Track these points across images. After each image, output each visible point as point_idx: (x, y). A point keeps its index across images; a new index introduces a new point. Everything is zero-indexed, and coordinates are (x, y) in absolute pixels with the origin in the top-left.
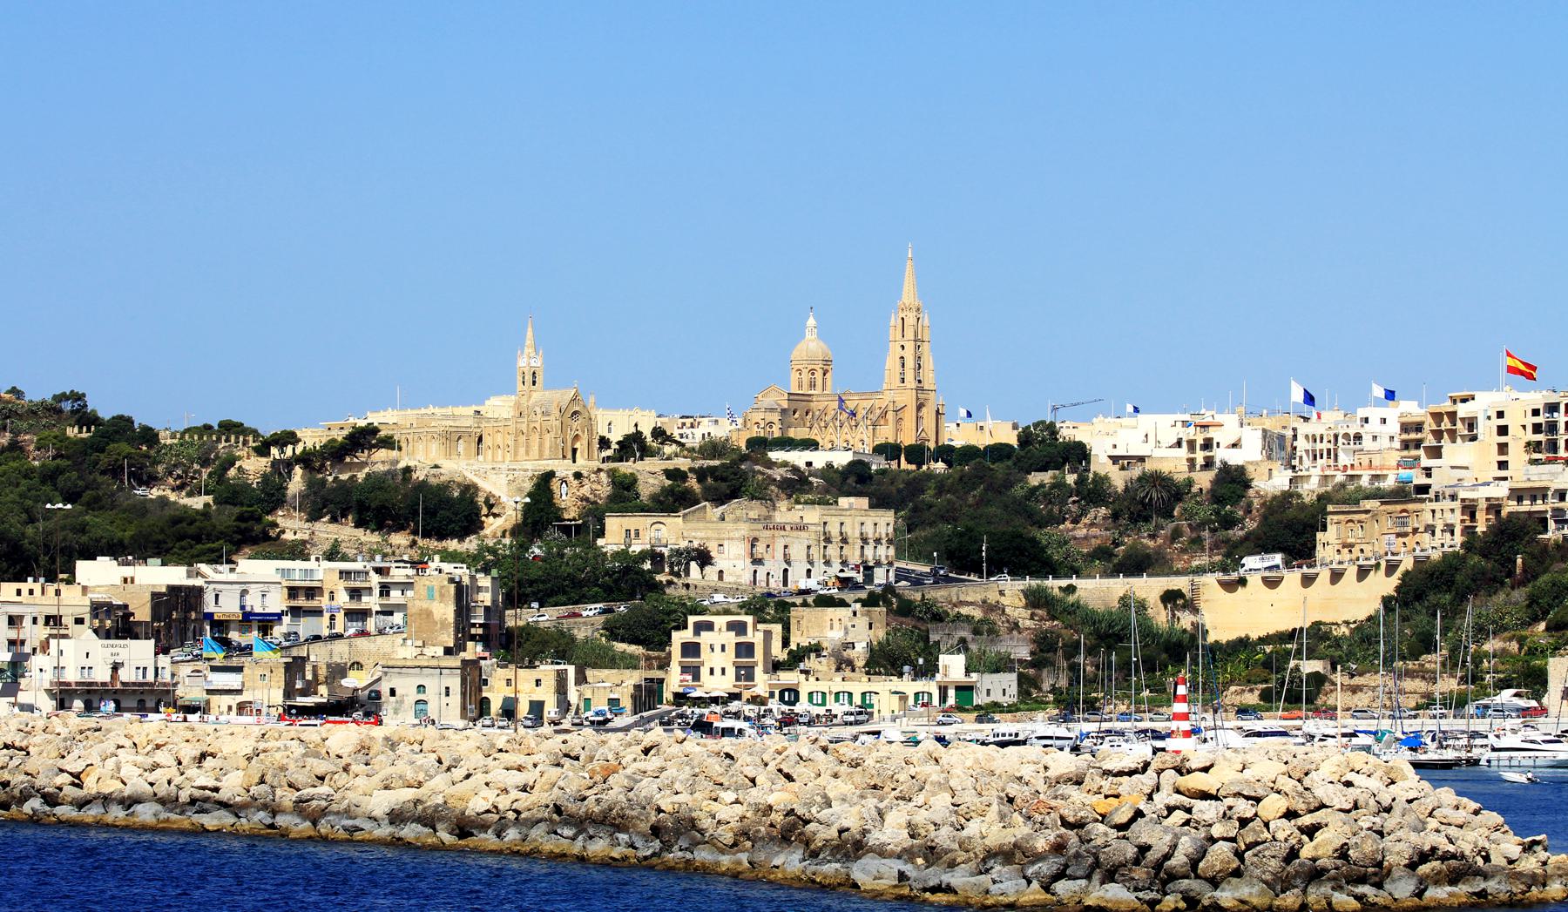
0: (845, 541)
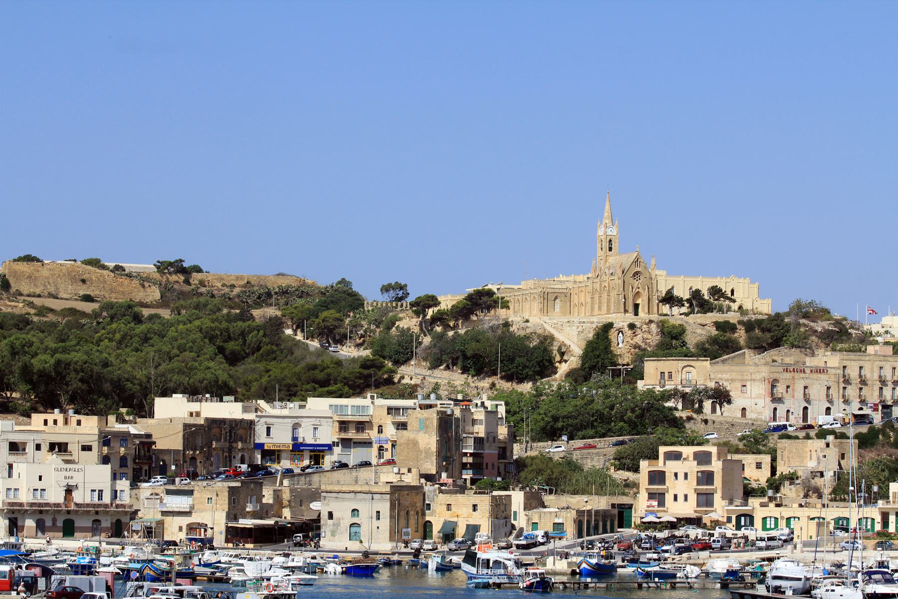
0: (863, 382)
